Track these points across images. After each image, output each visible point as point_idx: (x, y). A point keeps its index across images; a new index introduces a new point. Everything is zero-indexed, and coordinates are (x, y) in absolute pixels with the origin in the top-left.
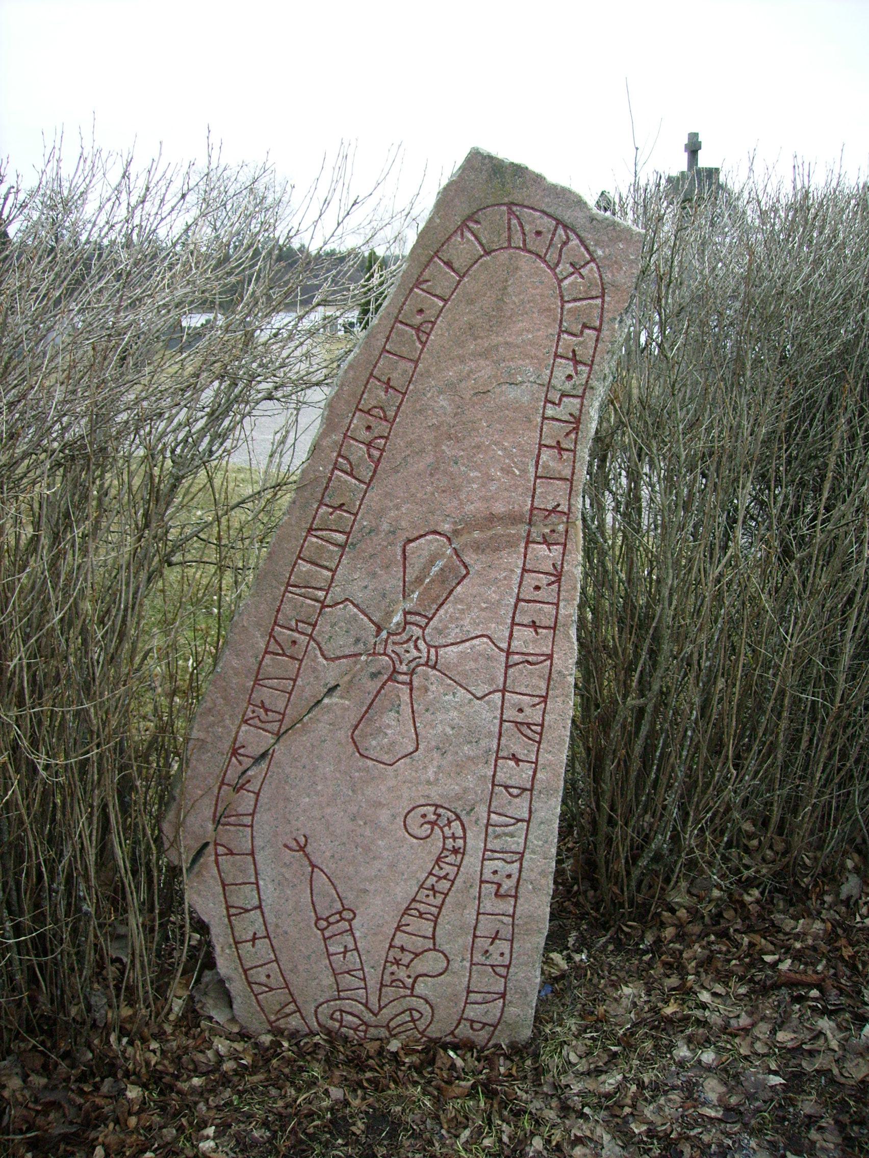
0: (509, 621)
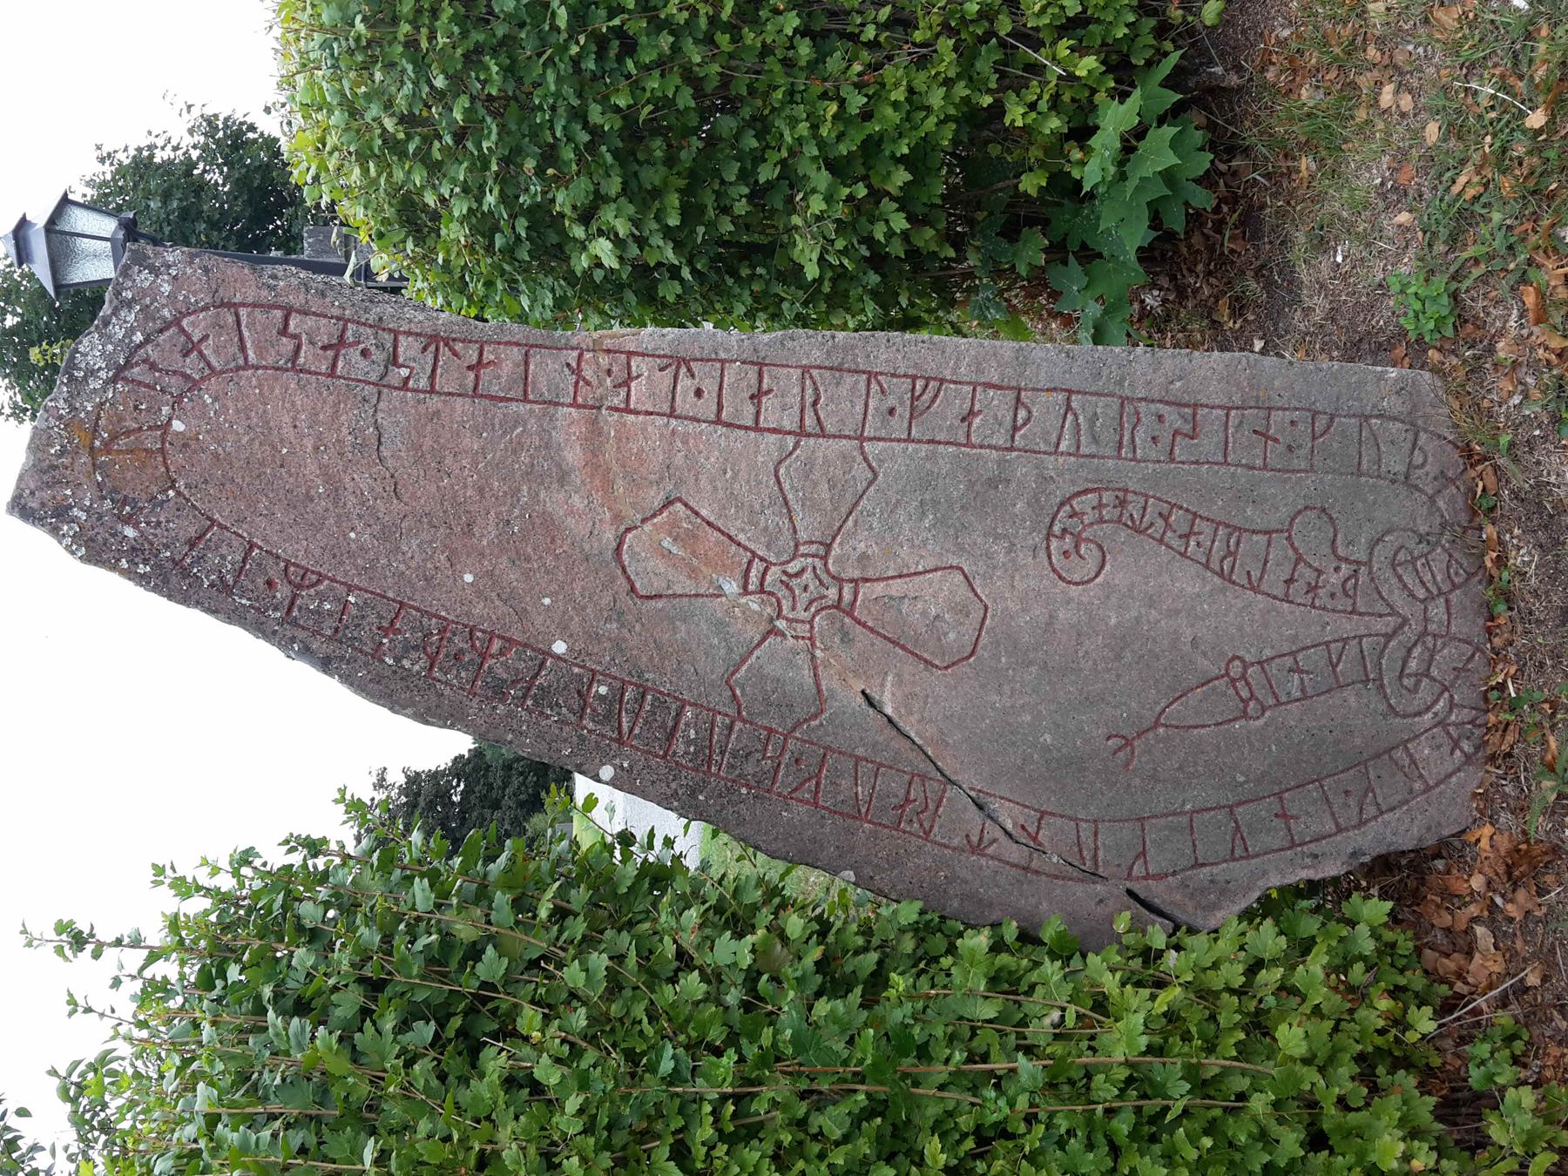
0: (752, 434)
